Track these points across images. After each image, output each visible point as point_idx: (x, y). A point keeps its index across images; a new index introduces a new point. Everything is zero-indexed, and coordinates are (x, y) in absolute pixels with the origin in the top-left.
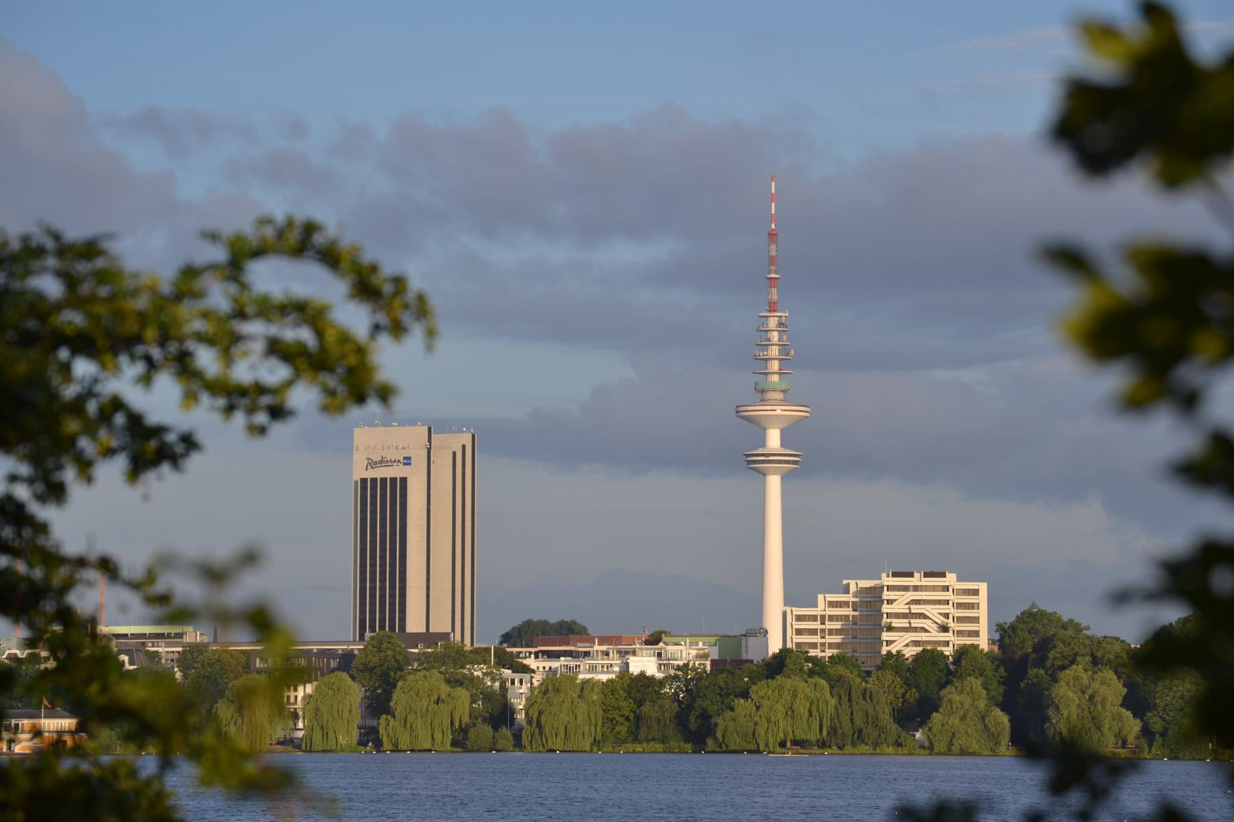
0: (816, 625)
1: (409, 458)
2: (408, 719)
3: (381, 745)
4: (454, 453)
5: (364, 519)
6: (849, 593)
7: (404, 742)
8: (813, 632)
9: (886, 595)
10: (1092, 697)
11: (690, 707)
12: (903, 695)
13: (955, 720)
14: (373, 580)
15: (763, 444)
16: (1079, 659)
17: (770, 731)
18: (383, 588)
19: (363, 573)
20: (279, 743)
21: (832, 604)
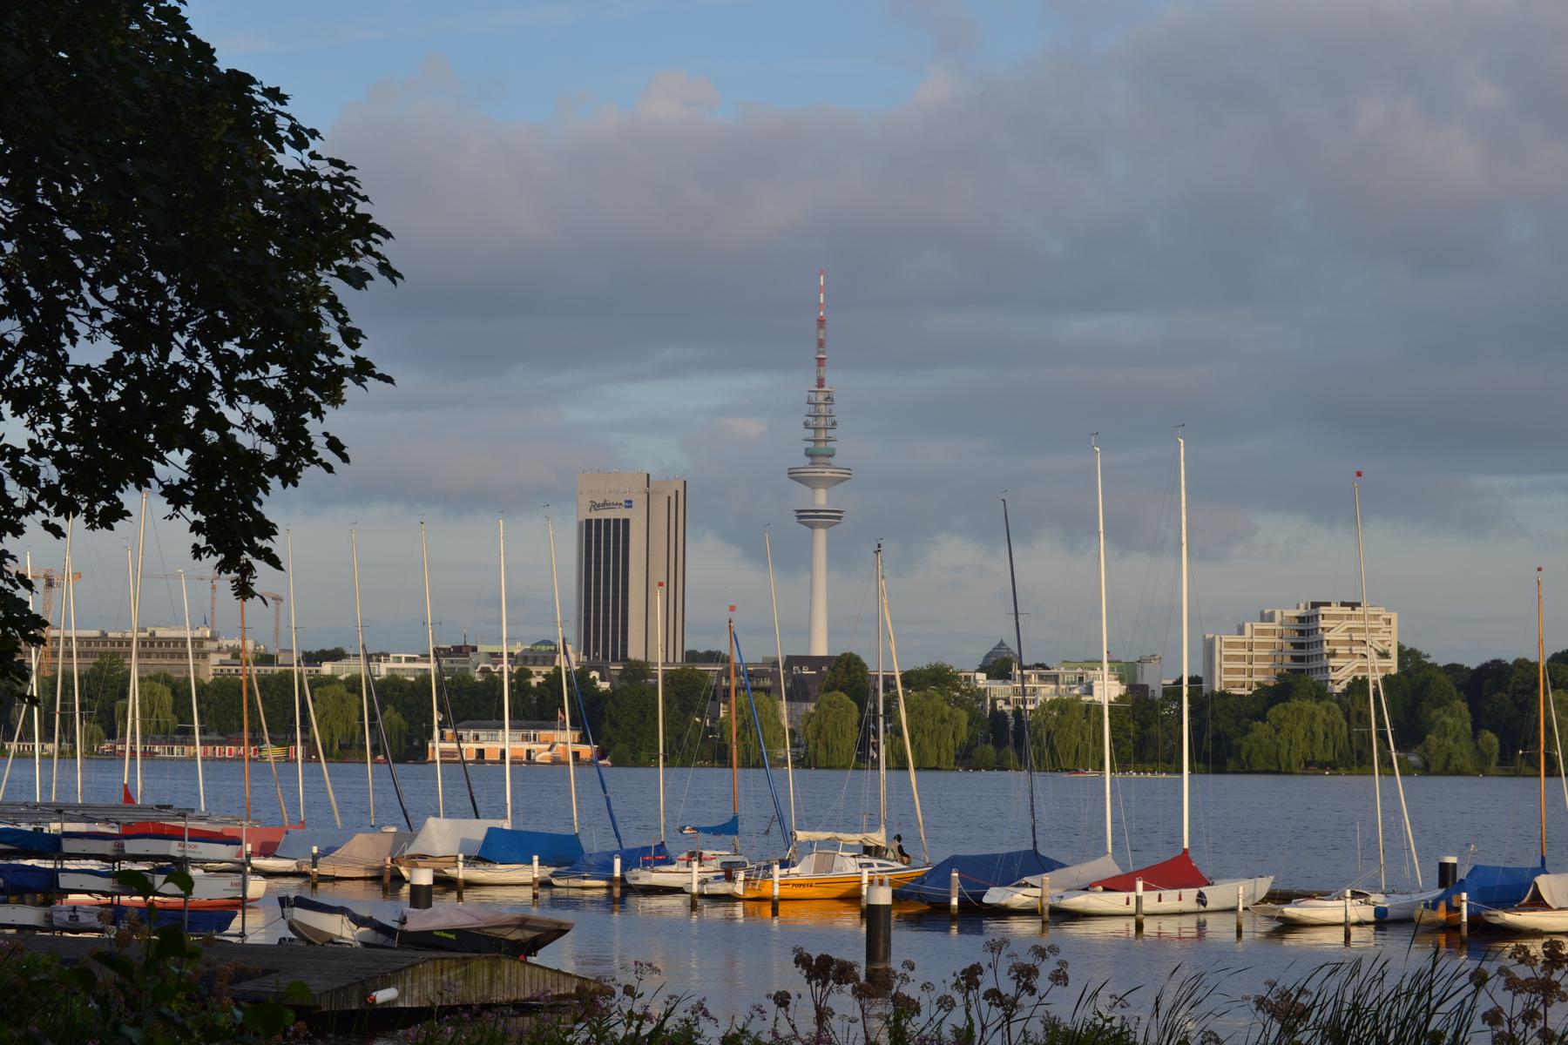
1: (630, 502)
2: (916, 738)
4: (669, 498)
6: (1274, 622)
13: (1449, 742)
17: (1292, 752)
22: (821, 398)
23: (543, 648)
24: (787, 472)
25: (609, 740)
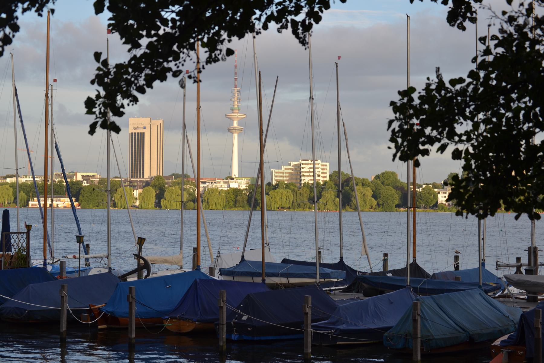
0: (281, 175)
1: (145, 127)
3: (162, 207)
4: (158, 126)
5: (132, 144)
7: (168, 206)
8: (280, 176)
9: (302, 166)
10: (364, 195)
11: (251, 198)
12: (309, 194)
14: (135, 162)
15: (233, 125)
16: (359, 184)
18: (137, 164)
19: (132, 159)
20: (132, 206)
21: (286, 169)
22: (236, 91)
23: (72, 174)
24: (225, 115)
25: (81, 201)
